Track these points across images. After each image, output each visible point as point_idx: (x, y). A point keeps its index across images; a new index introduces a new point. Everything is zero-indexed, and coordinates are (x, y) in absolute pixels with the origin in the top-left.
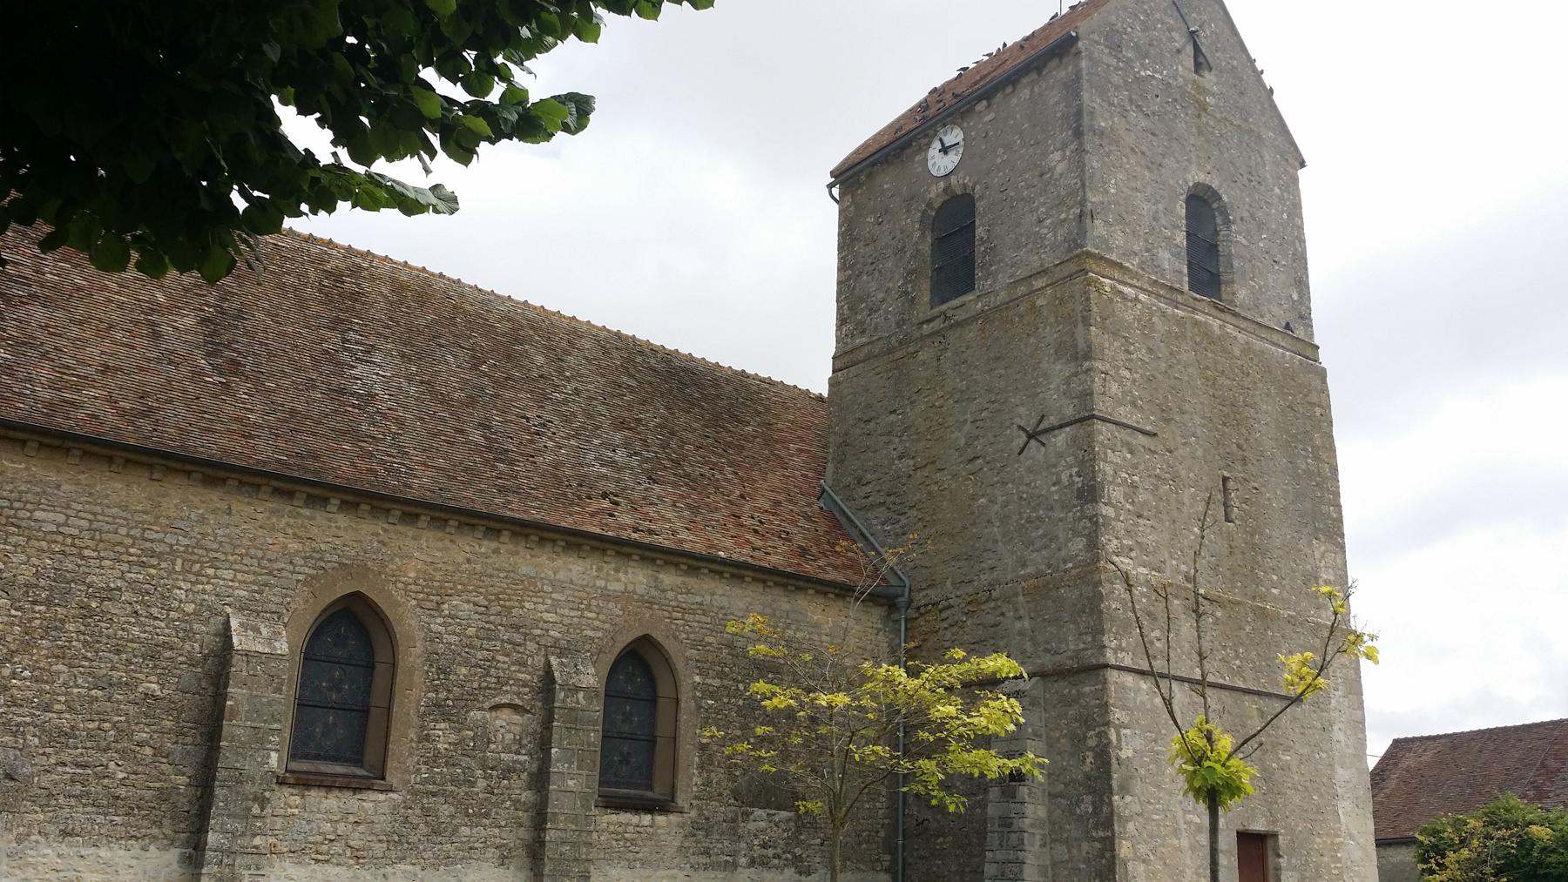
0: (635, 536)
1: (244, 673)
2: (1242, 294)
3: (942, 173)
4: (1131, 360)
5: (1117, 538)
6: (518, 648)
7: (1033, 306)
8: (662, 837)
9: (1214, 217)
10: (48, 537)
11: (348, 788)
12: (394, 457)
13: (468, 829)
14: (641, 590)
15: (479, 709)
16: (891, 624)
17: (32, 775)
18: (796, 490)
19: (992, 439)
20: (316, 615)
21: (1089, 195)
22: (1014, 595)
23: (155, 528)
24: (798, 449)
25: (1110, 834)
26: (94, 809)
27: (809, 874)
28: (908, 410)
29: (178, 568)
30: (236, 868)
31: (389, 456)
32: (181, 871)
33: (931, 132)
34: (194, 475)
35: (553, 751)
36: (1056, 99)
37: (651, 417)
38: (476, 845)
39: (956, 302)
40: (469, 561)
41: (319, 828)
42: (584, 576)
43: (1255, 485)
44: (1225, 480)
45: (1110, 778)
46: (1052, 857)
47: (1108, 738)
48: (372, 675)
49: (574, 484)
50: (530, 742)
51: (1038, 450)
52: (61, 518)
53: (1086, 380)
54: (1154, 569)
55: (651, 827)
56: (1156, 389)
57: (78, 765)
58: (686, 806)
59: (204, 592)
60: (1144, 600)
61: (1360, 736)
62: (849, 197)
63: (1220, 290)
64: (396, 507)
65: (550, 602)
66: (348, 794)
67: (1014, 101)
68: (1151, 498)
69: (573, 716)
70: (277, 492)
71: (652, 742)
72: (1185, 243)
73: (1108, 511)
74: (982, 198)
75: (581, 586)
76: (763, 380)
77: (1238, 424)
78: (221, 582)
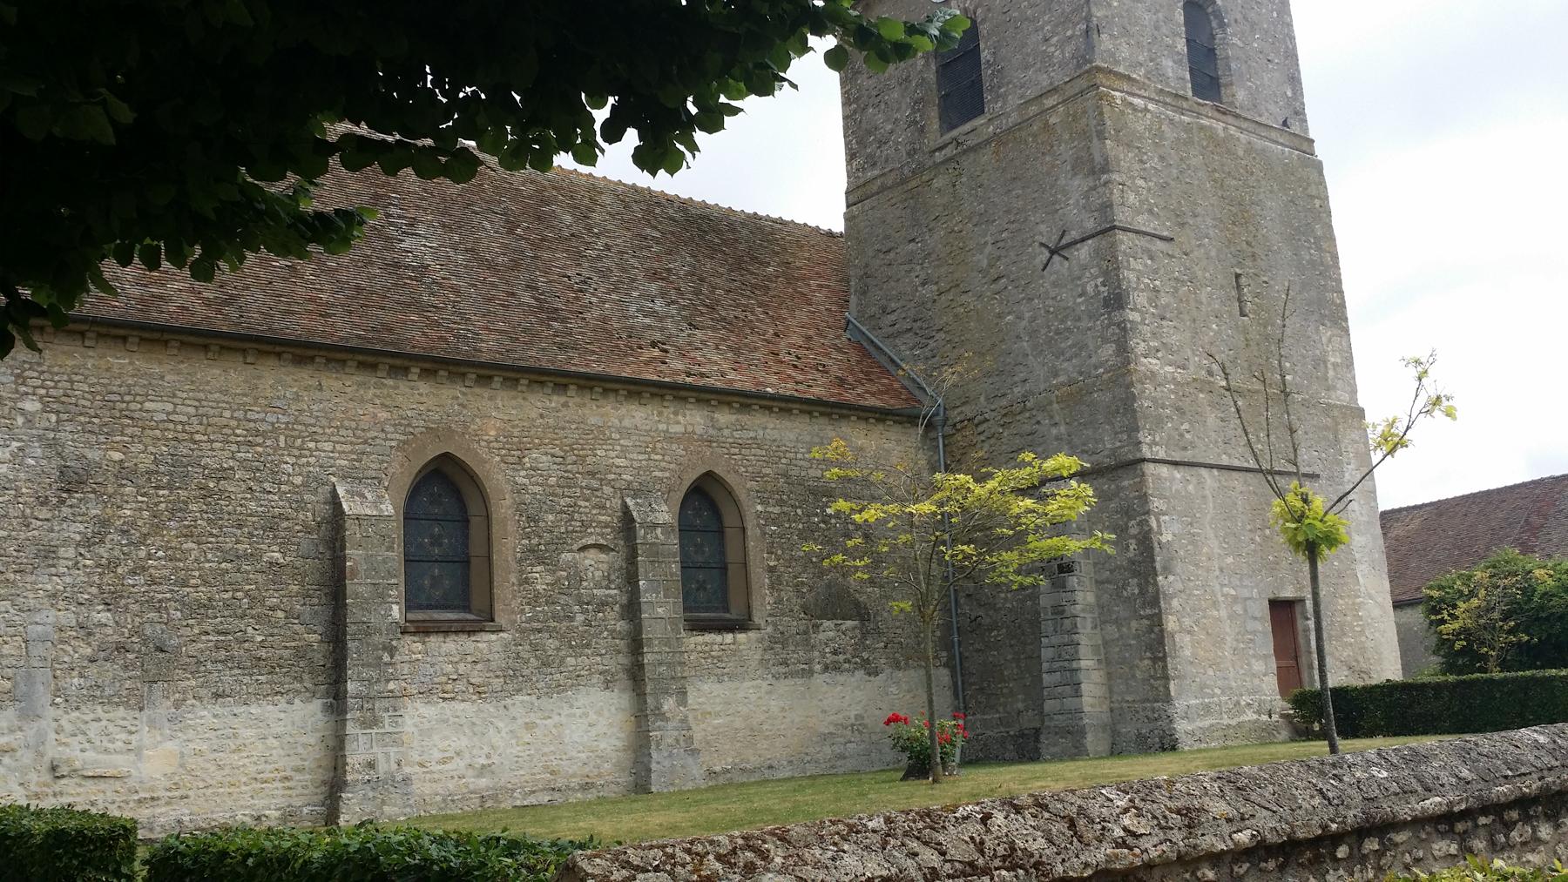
0: (689, 380)
1: (358, 535)
2: (1241, 95)
4: (1145, 169)
5: (1144, 341)
6: (596, 493)
8: (744, 653)
9: (1210, 22)
10: (161, 426)
11: (463, 632)
12: (459, 324)
13: (573, 659)
14: (699, 430)
15: (569, 551)
16: (928, 442)
17: (180, 646)
18: (823, 324)
20: (412, 478)
21: (1094, 10)
23: (255, 409)
24: (819, 285)
26: (240, 671)
27: (877, 674)
28: (927, 237)
29: (282, 444)
30: (376, 711)
31: (455, 323)
32: (326, 719)
34: (285, 356)
35: (641, 583)
37: (680, 265)
38: (582, 673)
39: (967, 127)
40: (542, 416)
41: (442, 669)
42: (647, 422)
43: (1265, 279)
44: (1238, 276)
45: (1154, 561)
46: (1103, 638)
47: (1149, 526)
48: (467, 528)
49: (624, 336)
50: (618, 578)
51: (1061, 265)
52: (170, 407)
53: (1104, 193)
54: (1179, 367)
55: (734, 644)
56: (1170, 195)
57: (219, 633)
59: (308, 464)
60: (1172, 397)
61: (1372, 504)
63: (1219, 93)
64: (472, 370)
65: (618, 448)
66: (464, 637)
68: (1172, 300)
69: (655, 552)
70: (362, 366)
71: (724, 569)
72: (1186, 50)
73: (1134, 316)
74: (984, 21)
76: (775, 221)
77: (1246, 223)
78: (323, 454)
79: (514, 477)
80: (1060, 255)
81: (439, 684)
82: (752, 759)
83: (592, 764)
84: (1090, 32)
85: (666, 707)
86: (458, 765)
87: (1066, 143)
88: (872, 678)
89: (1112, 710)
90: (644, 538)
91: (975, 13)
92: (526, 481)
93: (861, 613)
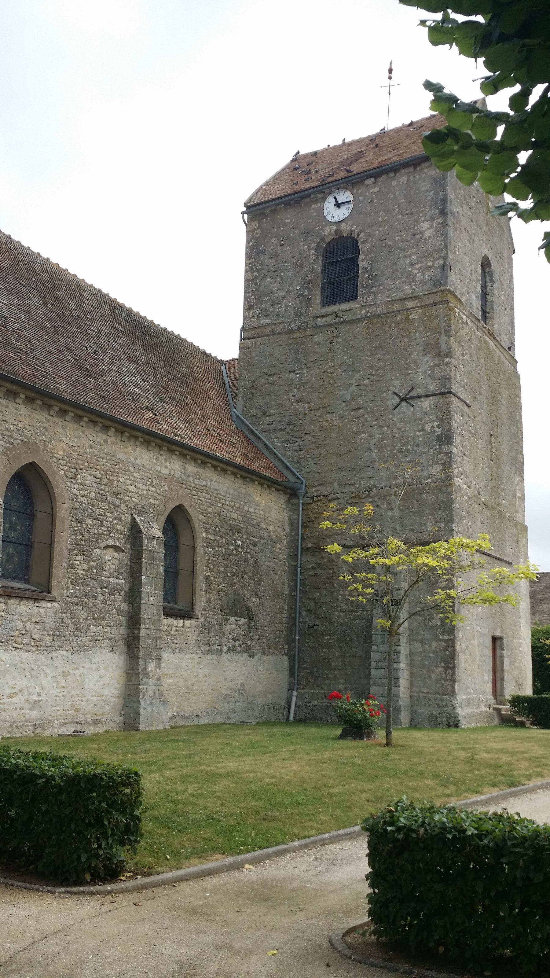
3: (335, 220)
7: (407, 318)
8: (188, 634)
11: (31, 599)
16: (290, 505)
19: (372, 398)
22: (388, 496)
25: (452, 638)
28: (305, 372)
33: (327, 191)
35: (143, 577)
36: (427, 187)
40: (91, 447)
42: (150, 463)
51: (408, 409)
53: (446, 370)
58: (200, 614)
62: (256, 223)
65: (132, 478)
67: (394, 183)
74: (365, 242)
75: (149, 469)
79: (71, 488)
80: (407, 402)
81: (13, 636)
82: (187, 709)
83: (99, 706)
84: (445, 267)
85: (150, 669)
86: (20, 699)
87: (421, 332)
88: (251, 659)
89: (411, 697)
90: (147, 546)
91: (358, 235)
92: (77, 492)
93: (249, 615)
